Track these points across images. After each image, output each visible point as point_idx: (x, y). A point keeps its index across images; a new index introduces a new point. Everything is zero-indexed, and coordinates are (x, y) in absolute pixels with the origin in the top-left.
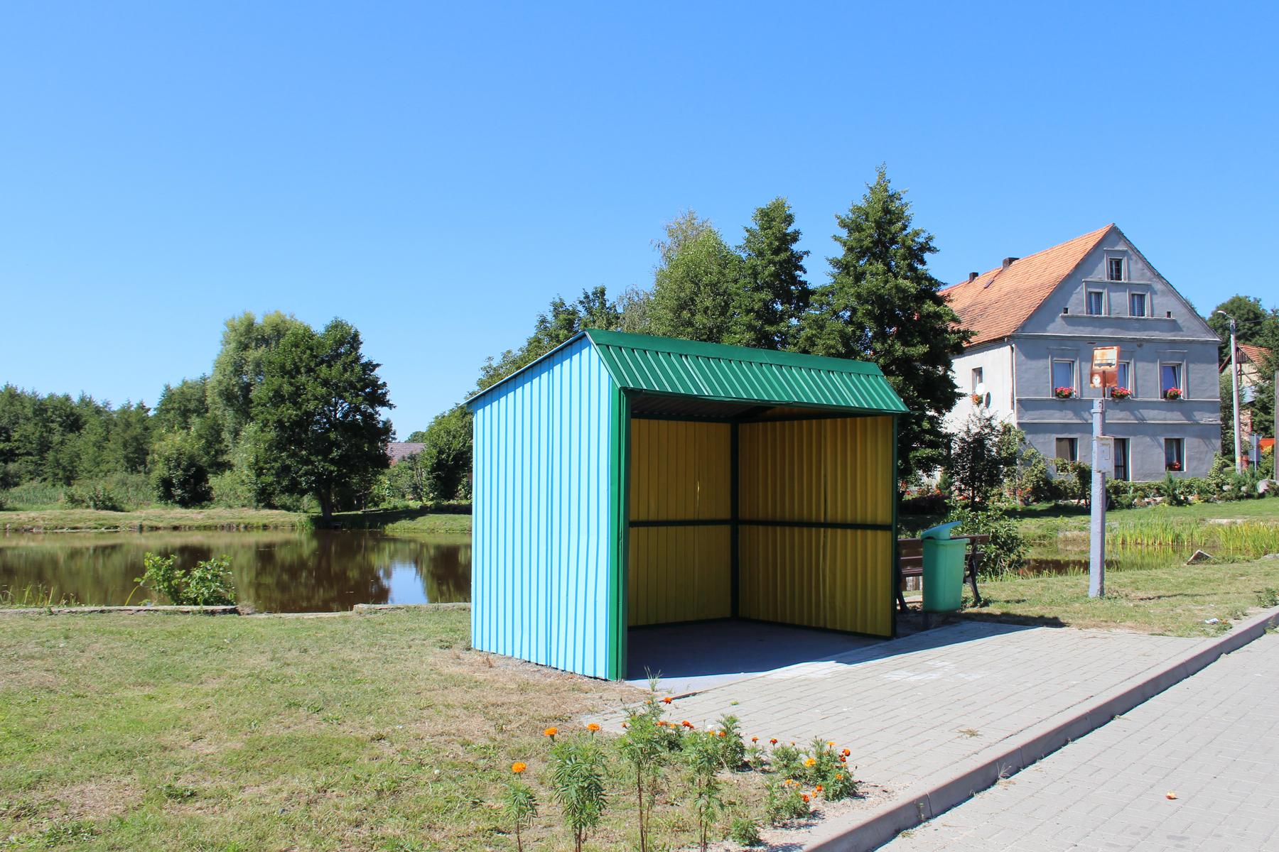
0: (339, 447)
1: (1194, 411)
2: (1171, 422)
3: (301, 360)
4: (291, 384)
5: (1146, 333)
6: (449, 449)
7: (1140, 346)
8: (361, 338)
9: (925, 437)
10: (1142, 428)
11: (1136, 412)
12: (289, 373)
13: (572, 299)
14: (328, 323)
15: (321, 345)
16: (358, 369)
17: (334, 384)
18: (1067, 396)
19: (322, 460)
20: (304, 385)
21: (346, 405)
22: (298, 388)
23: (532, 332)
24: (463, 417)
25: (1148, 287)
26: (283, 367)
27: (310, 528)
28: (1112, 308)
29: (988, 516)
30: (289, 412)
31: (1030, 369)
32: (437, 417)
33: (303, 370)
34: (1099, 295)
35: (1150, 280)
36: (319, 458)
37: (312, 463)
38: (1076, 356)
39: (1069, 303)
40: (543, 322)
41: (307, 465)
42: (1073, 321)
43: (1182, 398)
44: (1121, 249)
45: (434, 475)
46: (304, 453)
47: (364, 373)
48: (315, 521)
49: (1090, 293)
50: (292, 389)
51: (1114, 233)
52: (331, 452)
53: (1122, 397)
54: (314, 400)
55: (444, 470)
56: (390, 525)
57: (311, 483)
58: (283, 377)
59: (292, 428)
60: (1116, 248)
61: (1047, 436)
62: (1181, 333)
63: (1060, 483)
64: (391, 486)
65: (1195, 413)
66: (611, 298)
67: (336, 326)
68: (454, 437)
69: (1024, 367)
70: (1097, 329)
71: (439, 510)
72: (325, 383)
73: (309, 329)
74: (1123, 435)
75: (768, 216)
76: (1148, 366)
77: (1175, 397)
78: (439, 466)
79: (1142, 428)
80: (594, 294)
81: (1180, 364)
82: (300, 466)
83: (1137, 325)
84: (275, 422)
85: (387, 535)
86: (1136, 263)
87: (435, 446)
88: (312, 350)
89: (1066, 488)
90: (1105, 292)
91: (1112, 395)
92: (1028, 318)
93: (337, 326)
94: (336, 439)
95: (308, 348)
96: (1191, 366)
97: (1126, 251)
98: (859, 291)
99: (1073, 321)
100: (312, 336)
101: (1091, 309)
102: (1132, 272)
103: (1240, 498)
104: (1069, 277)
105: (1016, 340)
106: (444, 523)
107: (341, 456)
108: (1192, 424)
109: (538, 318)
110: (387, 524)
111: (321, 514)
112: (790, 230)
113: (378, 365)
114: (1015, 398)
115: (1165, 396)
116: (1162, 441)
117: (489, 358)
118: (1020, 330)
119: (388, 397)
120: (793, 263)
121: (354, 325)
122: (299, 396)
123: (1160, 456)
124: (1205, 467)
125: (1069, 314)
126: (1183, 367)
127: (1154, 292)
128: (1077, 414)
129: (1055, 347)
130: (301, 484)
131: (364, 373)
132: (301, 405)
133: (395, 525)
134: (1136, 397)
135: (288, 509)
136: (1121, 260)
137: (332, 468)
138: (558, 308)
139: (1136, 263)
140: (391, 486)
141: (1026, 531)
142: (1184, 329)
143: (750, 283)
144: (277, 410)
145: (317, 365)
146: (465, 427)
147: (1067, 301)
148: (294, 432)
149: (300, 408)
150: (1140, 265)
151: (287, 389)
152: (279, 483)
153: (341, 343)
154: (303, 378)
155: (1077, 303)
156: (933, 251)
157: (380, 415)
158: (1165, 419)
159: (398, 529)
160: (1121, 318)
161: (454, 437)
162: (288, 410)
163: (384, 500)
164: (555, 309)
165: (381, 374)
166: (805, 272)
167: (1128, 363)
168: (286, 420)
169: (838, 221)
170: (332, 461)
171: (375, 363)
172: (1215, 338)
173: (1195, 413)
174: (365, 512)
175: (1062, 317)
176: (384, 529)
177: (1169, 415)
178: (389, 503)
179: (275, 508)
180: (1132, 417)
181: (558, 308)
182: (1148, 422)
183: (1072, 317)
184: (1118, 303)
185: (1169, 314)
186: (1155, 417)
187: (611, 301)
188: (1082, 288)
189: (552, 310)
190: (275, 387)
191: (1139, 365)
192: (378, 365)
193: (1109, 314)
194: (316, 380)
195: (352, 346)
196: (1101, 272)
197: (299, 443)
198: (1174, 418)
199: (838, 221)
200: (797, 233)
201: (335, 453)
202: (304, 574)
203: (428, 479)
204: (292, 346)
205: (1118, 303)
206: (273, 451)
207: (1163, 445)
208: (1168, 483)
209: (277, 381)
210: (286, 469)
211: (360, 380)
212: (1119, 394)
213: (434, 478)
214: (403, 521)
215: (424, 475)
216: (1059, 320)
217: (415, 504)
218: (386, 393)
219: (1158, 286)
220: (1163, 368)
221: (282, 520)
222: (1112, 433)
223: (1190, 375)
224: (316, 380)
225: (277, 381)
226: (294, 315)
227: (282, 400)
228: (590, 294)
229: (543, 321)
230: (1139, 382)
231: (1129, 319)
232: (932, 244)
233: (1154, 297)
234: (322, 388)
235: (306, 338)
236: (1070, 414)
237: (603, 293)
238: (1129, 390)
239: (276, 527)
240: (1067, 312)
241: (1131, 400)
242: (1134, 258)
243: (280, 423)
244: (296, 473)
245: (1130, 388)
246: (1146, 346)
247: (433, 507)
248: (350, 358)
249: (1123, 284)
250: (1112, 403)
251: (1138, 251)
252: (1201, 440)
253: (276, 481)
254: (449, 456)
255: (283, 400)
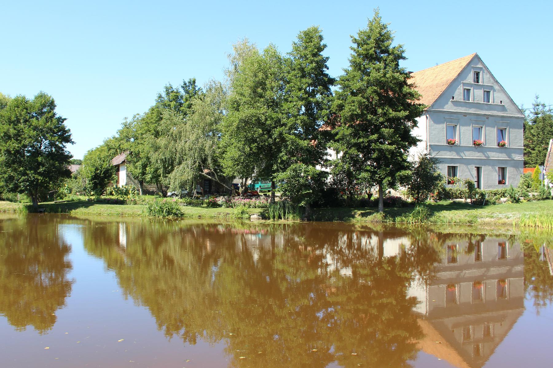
0: (43, 166)
1: (512, 153)
2: (501, 159)
3: (21, 115)
4: (15, 129)
5: (491, 112)
6: (101, 167)
7: (488, 118)
8: (55, 103)
9: (404, 164)
10: (488, 162)
11: (485, 153)
12: (13, 122)
13: (177, 85)
14: (36, 94)
15: (32, 107)
16: (54, 121)
17: (41, 129)
18: (453, 144)
19: (33, 173)
20: (22, 129)
21: (47, 142)
22: (19, 131)
23: (154, 104)
24: (109, 150)
25: (492, 87)
26: (10, 119)
27: (25, 212)
28: (475, 98)
29: (525, 215)
30: (13, 145)
31: (436, 128)
32: (89, 151)
33: (22, 121)
34: (468, 90)
35: (493, 84)
36: (32, 172)
37: (27, 175)
38: (458, 122)
39: (455, 94)
40: (160, 97)
41: (25, 176)
42: (456, 103)
43: (506, 146)
44: (480, 67)
45: (93, 182)
46: (21, 169)
47: (58, 124)
48: (28, 208)
49: (465, 89)
50: (16, 131)
51: (477, 58)
52: (39, 168)
53: (479, 145)
54: (29, 138)
55: (98, 179)
56: (73, 210)
57: (26, 187)
58: (10, 125)
59: (15, 154)
60: (478, 66)
61: (443, 165)
62: (507, 112)
63: (450, 190)
64: (68, 188)
65: (512, 155)
66: (199, 84)
67: (41, 96)
68: (104, 161)
69: (433, 127)
70: (468, 109)
71: (100, 202)
72: (35, 128)
73: (25, 97)
74: (479, 165)
75: (309, 36)
76: (492, 129)
77: (503, 145)
78: (96, 177)
79: (488, 162)
80: (190, 82)
81: (506, 129)
82: (20, 177)
83: (486, 107)
84: (5, 151)
85: (71, 217)
86: (486, 74)
87: (93, 166)
88: (27, 109)
89: (452, 193)
90: (472, 89)
91: (474, 144)
92: (435, 101)
93: (42, 96)
94: (42, 161)
95: (24, 108)
96: (511, 129)
97: (482, 68)
98: (369, 78)
99: (456, 103)
100: (26, 102)
101: (465, 99)
102: (484, 79)
103: (543, 199)
104: (455, 80)
105: (429, 113)
106: (106, 210)
107: (45, 171)
108: (511, 160)
109: (157, 95)
110: (71, 210)
111: (32, 204)
112: (322, 43)
113: (65, 119)
114: (428, 144)
115: (499, 145)
116: (497, 168)
117: (125, 118)
118: (431, 107)
119: (71, 138)
120: (321, 64)
121: (52, 96)
122: (20, 136)
123: (496, 177)
124: (516, 182)
125: (454, 100)
126: (507, 130)
127: (494, 91)
128: (458, 154)
129: (448, 118)
130: (20, 187)
131: (58, 124)
132: (21, 141)
133: (76, 211)
134: (486, 145)
135: (11, 201)
136: (479, 72)
137: (40, 178)
138: (169, 90)
139: (486, 74)
140: (68, 188)
141: (460, 218)
142: (508, 110)
143: (298, 73)
144: (6, 144)
145: (30, 118)
146: (110, 156)
147: (454, 93)
148: (16, 157)
149: (20, 143)
150: (488, 75)
151: (12, 131)
152: (7, 186)
153: (44, 106)
154: (21, 126)
155: (459, 95)
156: (404, 59)
157: (66, 148)
158: (498, 157)
159: (79, 212)
160: (479, 103)
161: (104, 161)
162: (13, 143)
163: (66, 196)
164: (167, 90)
165: (67, 125)
166: (328, 69)
167: (482, 127)
168: (12, 150)
169: (352, 39)
170: (40, 174)
171: (63, 118)
172: (522, 115)
173: (512, 155)
174: (56, 202)
175: (452, 101)
176: (70, 213)
177: (500, 155)
178: (69, 197)
179: (4, 200)
180: (483, 156)
181: (169, 90)
182: (491, 158)
183: (456, 101)
184: (477, 95)
185: (501, 102)
186: (495, 156)
187: (198, 87)
188: (461, 86)
189: (165, 91)
190: (5, 131)
191: (487, 128)
192: (65, 119)
193: (474, 101)
194: (30, 127)
195: (51, 109)
196: (470, 78)
197: (20, 163)
198: (503, 156)
199: (352, 39)
200: (325, 46)
201: (41, 169)
202: (22, 239)
203: (89, 184)
204: (15, 107)
205: (477, 95)
206: (3, 168)
207: (498, 171)
208: (511, 191)
209: (6, 127)
210: (11, 178)
211: (56, 127)
212: (478, 143)
213: (93, 183)
214: (81, 208)
215: (87, 182)
216: (450, 103)
217: (85, 198)
218: (70, 135)
219: (496, 87)
220: (498, 129)
221: (8, 207)
222: (474, 164)
223: (510, 134)
224: (30, 127)
225: (6, 127)
226: (10, 95)
227: (9, 138)
228: (187, 82)
229: (160, 97)
230: (487, 137)
231: (483, 104)
232: (404, 55)
233: (495, 93)
234: (34, 132)
235: (24, 103)
236: (454, 153)
237: (194, 82)
238: (482, 141)
239: (5, 211)
240: (453, 99)
241: (483, 147)
242: (485, 71)
243: (8, 152)
244: (18, 180)
245: (482, 140)
246: (490, 118)
247: (95, 200)
248: (50, 115)
249: (480, 85)
250: (474, 148)
251: (488, 68)
252: (515, 169)
253: (5, 185)
254: (101, 172)
255: (9, 138)
